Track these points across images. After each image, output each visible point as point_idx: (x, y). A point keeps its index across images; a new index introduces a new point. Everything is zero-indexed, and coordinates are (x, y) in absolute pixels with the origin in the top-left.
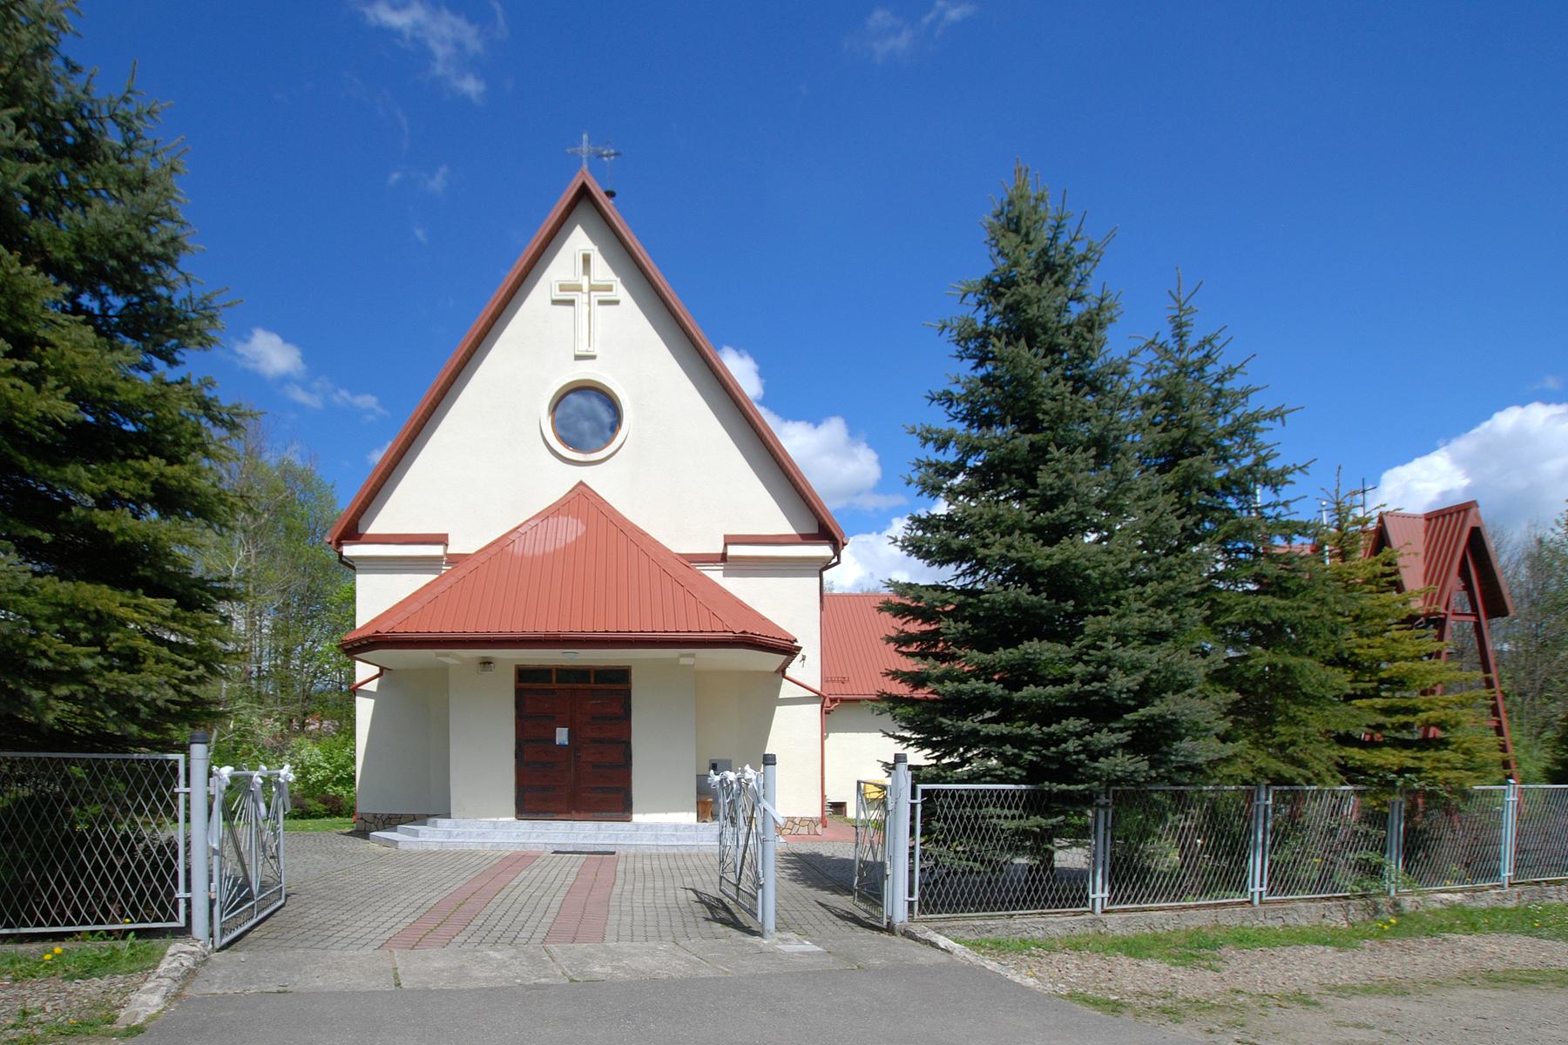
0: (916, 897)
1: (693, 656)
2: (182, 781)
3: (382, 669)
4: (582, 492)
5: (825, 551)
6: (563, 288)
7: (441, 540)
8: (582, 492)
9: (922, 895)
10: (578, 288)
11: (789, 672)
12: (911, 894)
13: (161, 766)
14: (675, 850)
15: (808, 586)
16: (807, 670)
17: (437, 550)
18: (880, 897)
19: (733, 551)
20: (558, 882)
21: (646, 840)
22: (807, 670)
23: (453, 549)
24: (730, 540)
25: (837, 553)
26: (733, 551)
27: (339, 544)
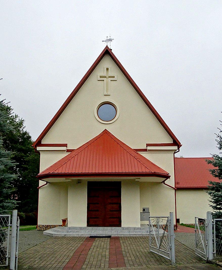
0: (215, 252)
1: (140, 179)
2: (10, 223)
3: (47, 182)
4: (106, 132)
5: (175, 148)
6: (101, 77)
7: (65, 145)
8: (106, 132)
9: (217, 251)
10: (105, 77)
11: (166, 182)
12: (213, 251)
13: (4, 218)
14: (135, 236)
15: (170, 156)
16: (171, 182)
17: (64, 148)
18: (10, 266)
19: (149, 148)
20: (38, 247)
21: (126, 233)
22: (171, 182)
23: (69, 148)
24: (148, 145)
25: (178, 149)
26: (149, 148)
27: (36, 147)
